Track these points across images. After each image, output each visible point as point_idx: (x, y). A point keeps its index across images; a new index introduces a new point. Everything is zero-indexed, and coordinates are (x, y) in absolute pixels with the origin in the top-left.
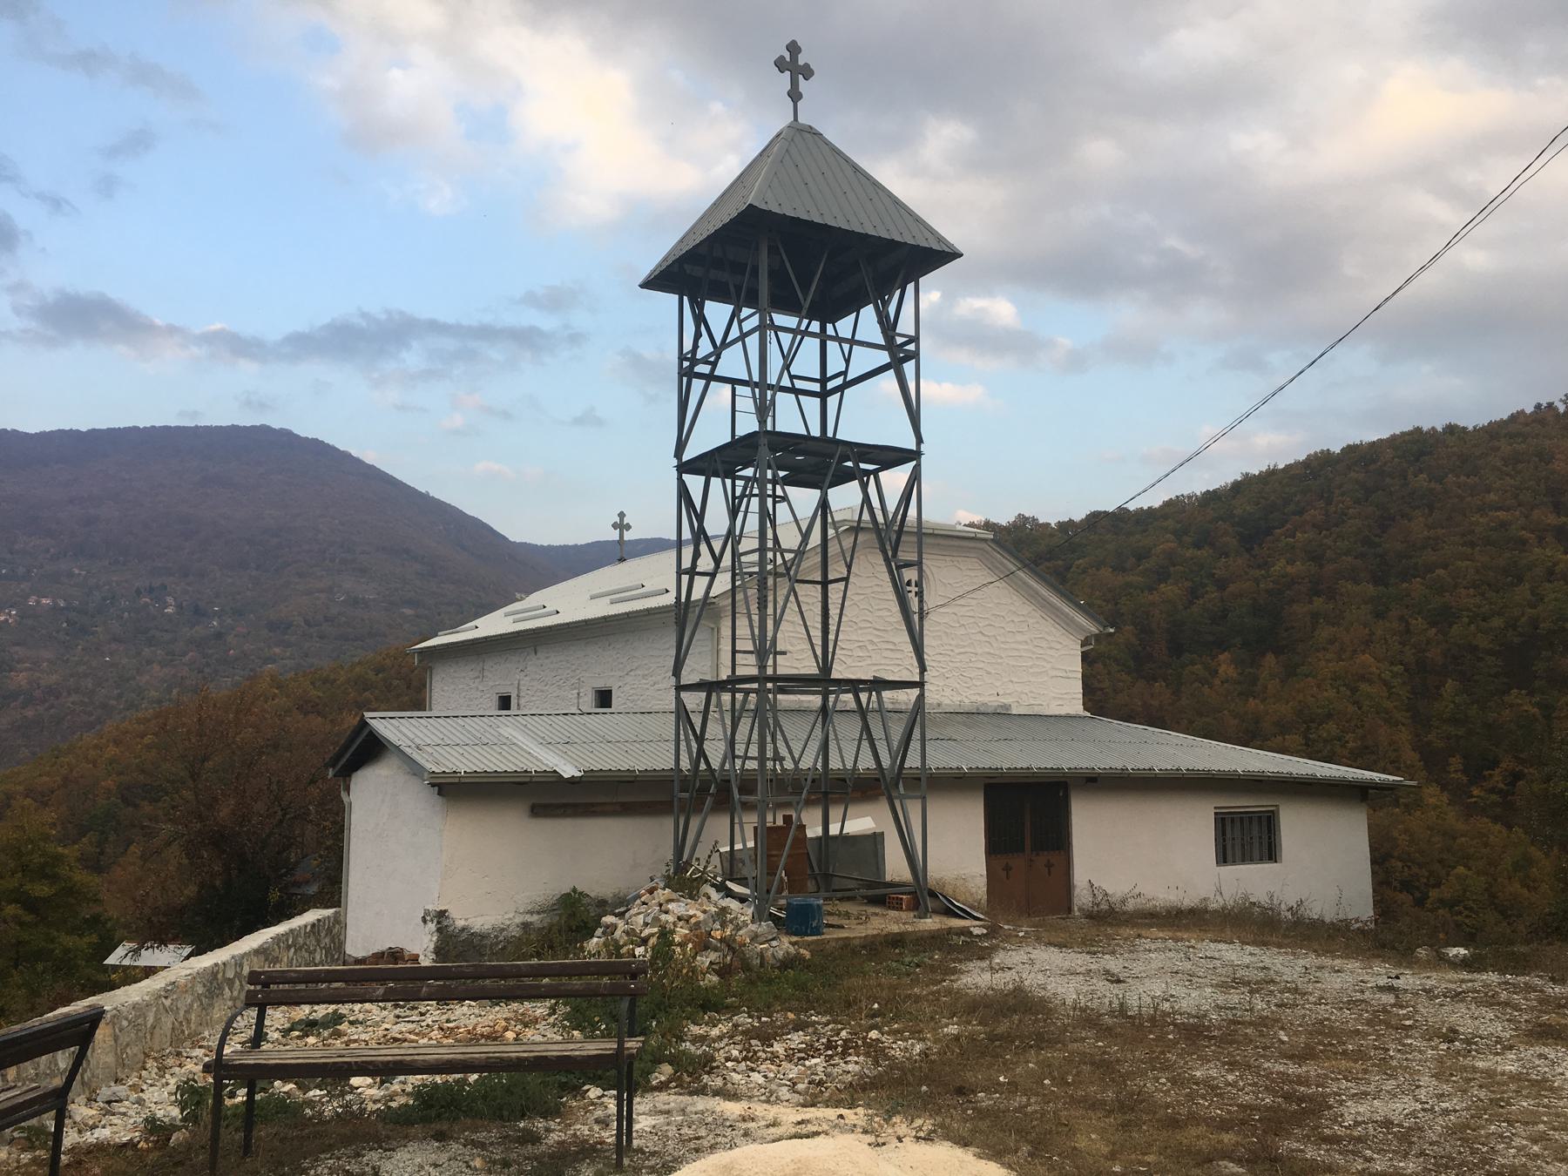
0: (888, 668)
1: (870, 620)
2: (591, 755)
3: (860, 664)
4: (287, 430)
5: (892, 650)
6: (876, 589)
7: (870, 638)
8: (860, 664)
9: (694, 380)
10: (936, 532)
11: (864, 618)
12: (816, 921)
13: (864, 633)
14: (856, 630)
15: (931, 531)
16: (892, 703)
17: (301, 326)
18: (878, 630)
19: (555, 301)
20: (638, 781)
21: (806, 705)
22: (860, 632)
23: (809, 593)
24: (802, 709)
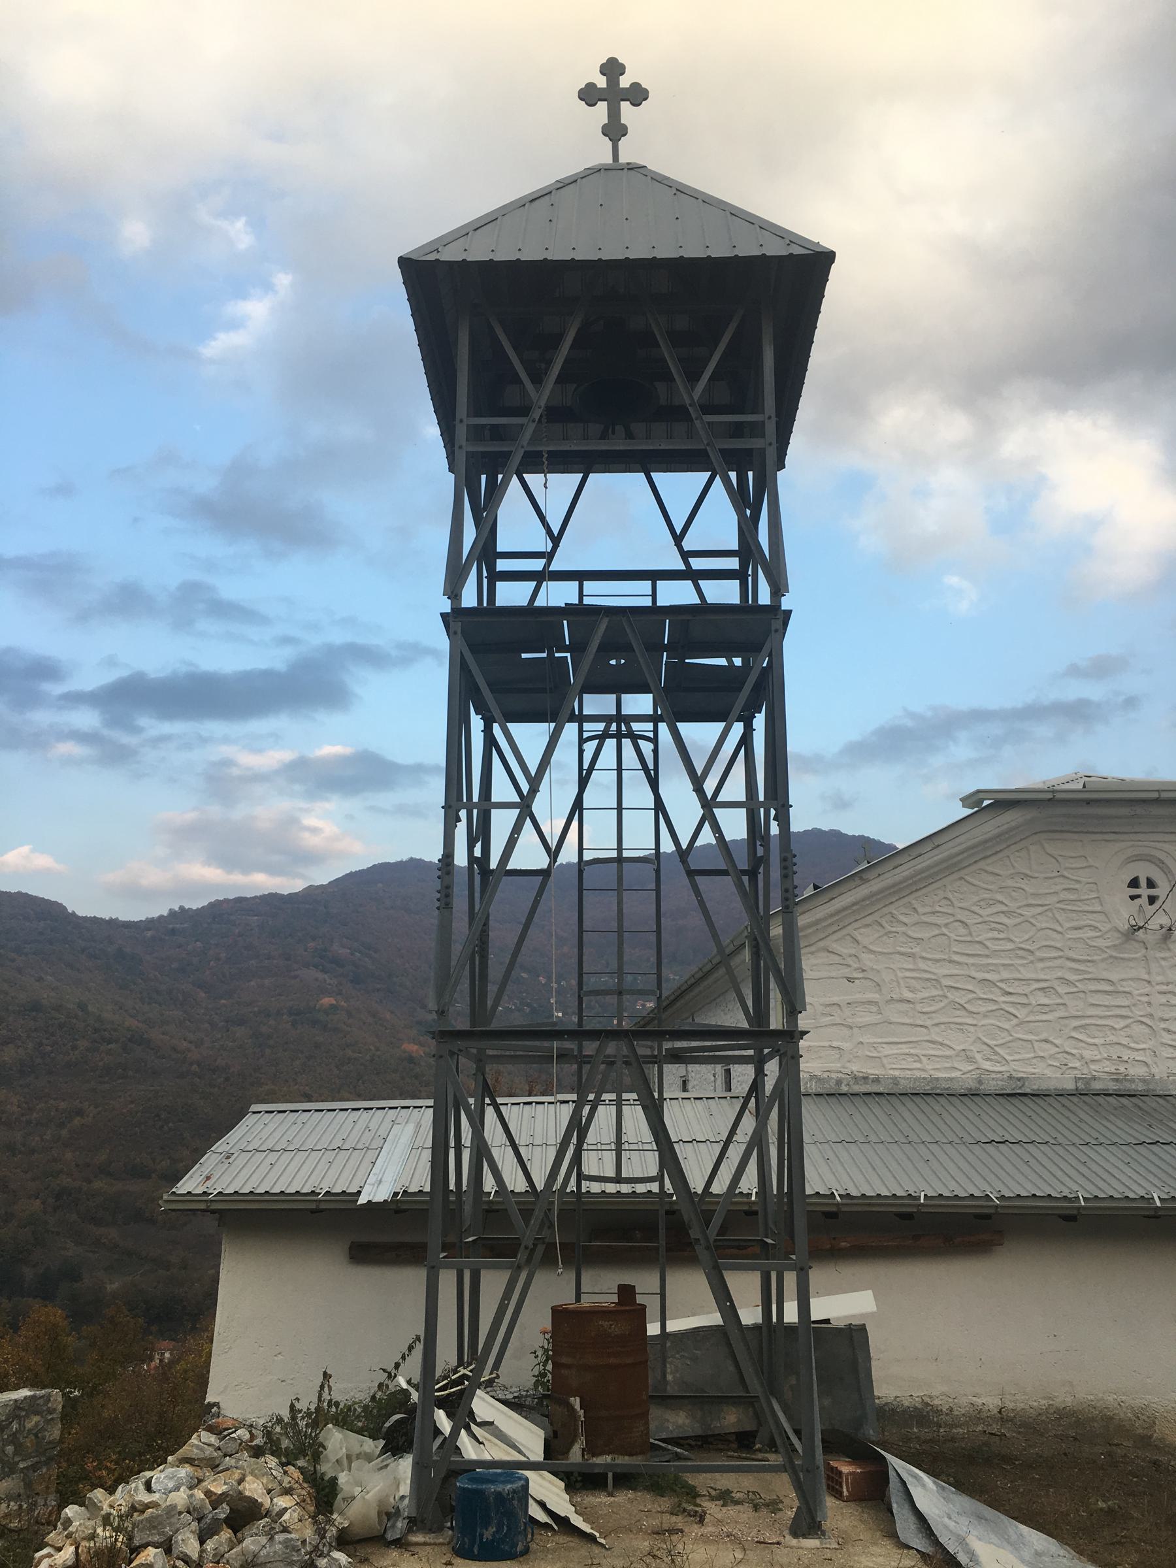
0: (1100, 1022)
1: (1058, 945)
2: (1025, 1168)
3: (1044, 1017)
4: (835, 830)
5: (1106, 992)
6: (1064, 895)
7: (1060, 974)
8: (1044, 1017)
9: (498, 584)
10: (1164, 795)
11: (1047, 943)
12: (493, 1530)
13: (1049, 968)
14: (1032, 962)
15: (1155, 795)
16: (1117, 1080)
17: (854, 736)
18: (1074, 960)
19: (1101, 668)
20: (322, 1211)
21: (945, 1085)
22: (1040, 965)
23: (938, 909)
24: (938, 1091)
